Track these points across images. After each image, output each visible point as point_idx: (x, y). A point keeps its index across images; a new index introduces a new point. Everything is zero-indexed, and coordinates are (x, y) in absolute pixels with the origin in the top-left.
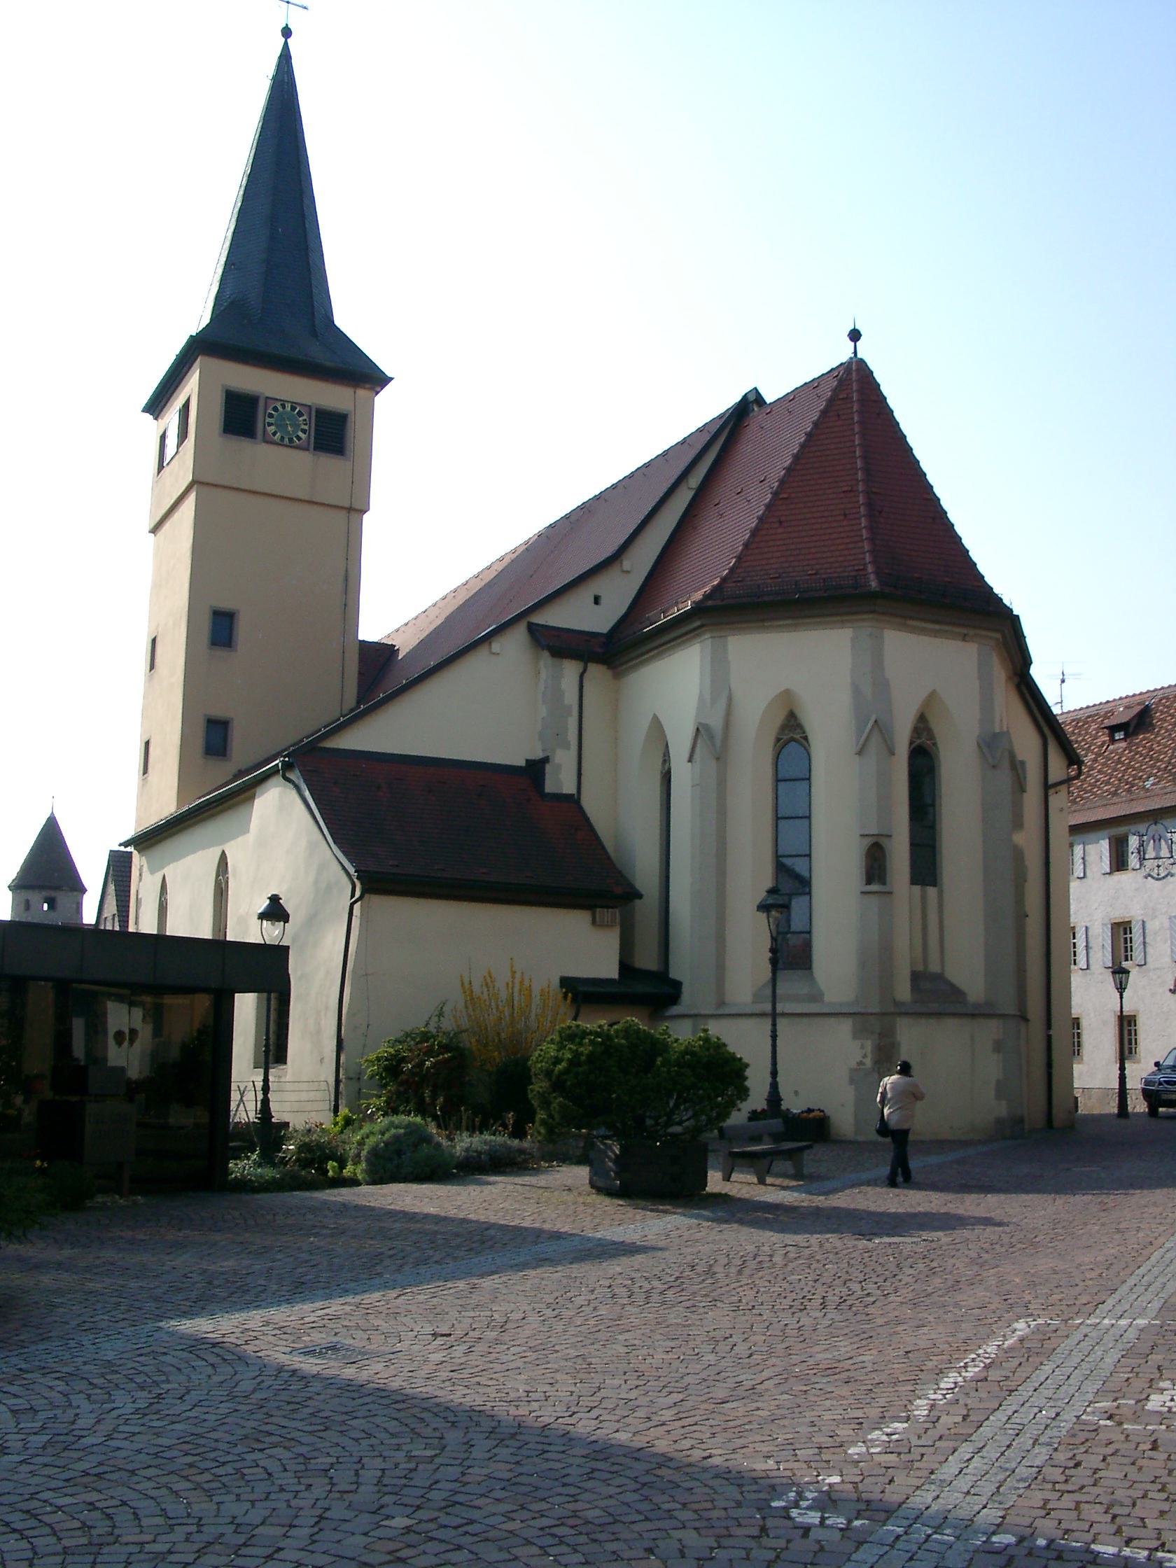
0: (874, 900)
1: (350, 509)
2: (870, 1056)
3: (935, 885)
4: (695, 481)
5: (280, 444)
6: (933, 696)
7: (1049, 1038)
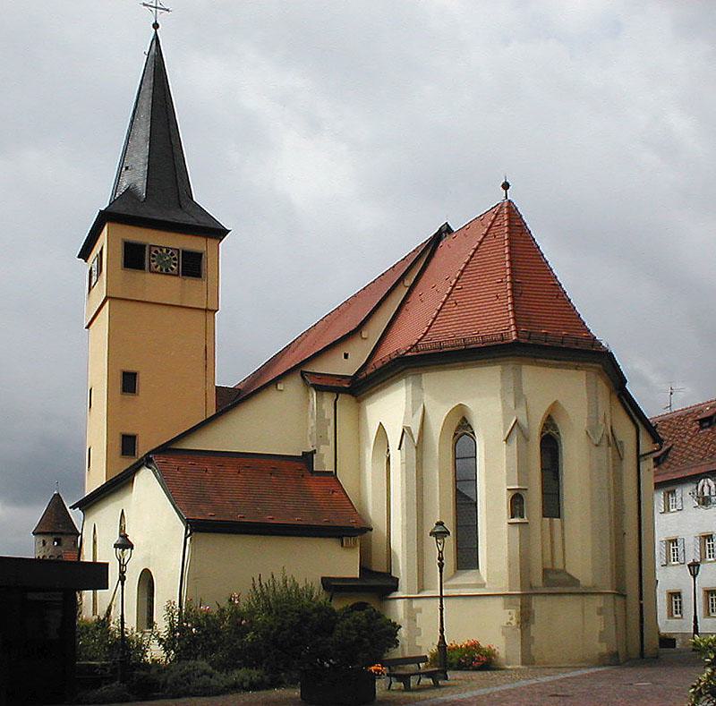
0: (517, 529)
1: (206, 310)
2: (515, 619)
3: (559, 517)
4: (408, 283)
5: (160, 273)
6: (555, 404)
7: (641, 605)
